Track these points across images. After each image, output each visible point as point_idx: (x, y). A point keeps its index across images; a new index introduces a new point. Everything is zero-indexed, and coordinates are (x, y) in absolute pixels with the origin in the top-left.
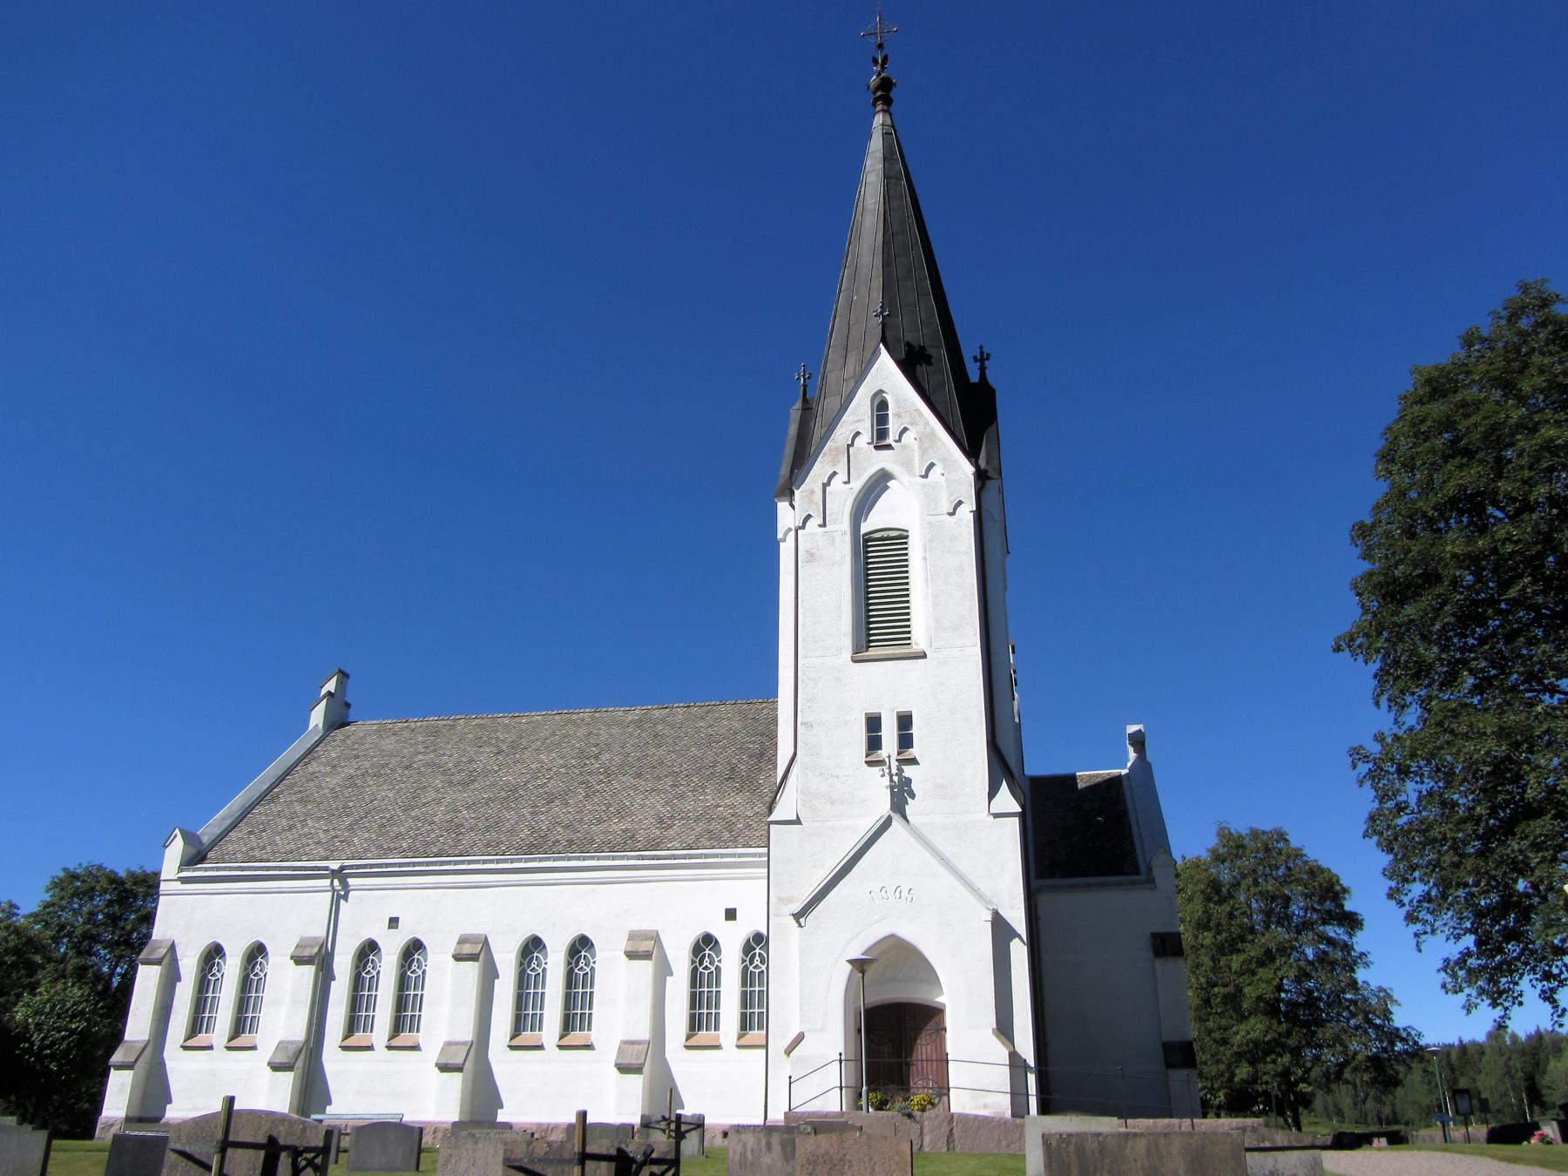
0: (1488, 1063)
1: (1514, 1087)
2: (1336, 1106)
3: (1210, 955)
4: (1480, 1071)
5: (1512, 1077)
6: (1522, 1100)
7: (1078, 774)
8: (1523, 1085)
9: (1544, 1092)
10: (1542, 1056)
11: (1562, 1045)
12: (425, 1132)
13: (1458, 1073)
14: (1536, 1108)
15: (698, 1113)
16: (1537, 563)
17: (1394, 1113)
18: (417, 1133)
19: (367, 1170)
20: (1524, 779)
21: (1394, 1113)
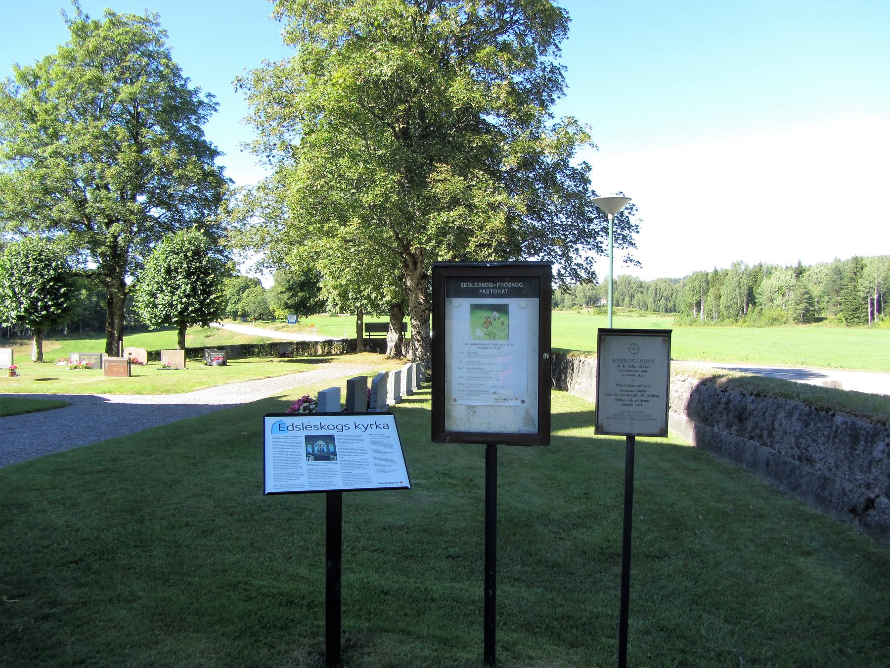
1: (740, 294)
2: (644, 302)
3: (294, 259)
5: (740, 288)
7: (637, 438)
8: (745, 292)
9: (757, 296)
10: (759, 277)
11: (772, 271)
14: (750, 305)
17: (675, 306)
18: (321, 506)
19: (340, 341)
20: (135, 151)
21: (675, 306)
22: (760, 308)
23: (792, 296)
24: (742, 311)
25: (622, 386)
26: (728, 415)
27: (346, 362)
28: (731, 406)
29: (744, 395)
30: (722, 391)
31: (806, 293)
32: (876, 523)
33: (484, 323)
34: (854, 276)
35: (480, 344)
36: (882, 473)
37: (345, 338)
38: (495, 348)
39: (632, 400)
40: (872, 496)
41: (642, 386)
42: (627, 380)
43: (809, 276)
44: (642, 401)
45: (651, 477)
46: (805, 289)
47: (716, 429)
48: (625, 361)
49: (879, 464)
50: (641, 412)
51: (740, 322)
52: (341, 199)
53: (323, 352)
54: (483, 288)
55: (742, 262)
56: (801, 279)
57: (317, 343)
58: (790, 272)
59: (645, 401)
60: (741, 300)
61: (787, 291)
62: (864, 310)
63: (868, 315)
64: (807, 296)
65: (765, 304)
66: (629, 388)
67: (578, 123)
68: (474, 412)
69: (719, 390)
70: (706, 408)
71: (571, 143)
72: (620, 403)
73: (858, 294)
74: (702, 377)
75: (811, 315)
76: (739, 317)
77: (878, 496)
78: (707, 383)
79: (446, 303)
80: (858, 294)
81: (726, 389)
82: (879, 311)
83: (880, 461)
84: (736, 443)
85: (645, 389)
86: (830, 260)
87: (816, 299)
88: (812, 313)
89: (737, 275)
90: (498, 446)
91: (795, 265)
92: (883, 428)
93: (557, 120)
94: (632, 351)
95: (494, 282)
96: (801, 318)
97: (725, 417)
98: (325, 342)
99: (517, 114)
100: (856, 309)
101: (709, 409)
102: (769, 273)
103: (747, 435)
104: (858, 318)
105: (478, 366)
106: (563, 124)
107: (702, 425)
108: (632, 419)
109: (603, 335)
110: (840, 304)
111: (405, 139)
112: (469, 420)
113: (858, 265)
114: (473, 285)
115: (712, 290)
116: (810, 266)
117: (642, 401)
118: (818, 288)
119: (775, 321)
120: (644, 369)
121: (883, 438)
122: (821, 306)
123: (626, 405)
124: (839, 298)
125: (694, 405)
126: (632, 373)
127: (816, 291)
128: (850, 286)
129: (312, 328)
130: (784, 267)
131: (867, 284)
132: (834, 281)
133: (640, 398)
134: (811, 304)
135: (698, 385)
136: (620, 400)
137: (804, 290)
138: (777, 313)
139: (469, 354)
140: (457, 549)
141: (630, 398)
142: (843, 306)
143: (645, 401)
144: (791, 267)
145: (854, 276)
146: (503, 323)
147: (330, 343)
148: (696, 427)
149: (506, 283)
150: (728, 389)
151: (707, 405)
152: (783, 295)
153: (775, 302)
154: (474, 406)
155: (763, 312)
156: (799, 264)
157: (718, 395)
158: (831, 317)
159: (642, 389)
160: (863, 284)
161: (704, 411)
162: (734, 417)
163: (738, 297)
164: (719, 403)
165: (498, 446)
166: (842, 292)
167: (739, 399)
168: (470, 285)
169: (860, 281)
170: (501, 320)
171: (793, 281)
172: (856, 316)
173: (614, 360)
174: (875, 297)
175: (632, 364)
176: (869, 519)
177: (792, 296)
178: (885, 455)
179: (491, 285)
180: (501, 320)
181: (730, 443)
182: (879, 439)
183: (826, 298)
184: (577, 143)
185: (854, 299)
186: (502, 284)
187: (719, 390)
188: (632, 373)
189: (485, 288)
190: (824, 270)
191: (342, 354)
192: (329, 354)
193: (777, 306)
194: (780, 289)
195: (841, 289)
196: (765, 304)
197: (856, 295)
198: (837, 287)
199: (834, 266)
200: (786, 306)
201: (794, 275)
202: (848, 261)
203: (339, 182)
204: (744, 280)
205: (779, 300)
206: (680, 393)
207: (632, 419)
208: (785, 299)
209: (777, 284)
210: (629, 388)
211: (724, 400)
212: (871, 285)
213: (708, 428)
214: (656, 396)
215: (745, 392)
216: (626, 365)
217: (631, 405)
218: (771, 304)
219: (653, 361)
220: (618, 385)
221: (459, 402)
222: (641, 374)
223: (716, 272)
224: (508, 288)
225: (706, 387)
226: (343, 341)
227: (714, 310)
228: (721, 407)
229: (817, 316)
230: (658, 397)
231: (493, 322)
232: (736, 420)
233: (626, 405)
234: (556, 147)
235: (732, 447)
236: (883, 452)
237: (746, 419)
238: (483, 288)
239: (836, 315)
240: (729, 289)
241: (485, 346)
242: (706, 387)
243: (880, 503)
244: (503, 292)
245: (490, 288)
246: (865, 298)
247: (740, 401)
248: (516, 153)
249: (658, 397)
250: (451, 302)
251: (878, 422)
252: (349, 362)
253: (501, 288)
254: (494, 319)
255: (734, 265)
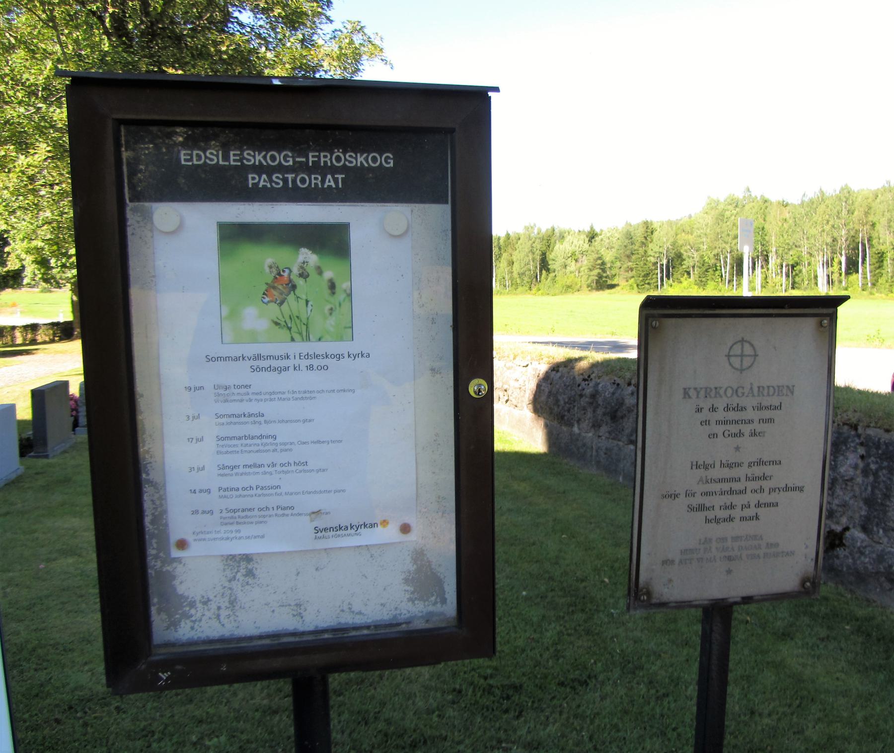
0: (521, 244)
4: (516, 250)
5: (533, 253)
6: (537, 267)
8: (538, 258)
9: (550, 262)
10: (552, 241)
11: (565, 235)
12: (222, 435)
13: (502, 251)
14: (544, 272)
15: (832, 188)
16: (171, 71)
19: (50, 324)
22: (554, 274)
23: (585, 262)
24: (536, 279)
25: (706, 467)
26: (594, 411)
27: (57, 352)
28: (600, 400)
29: (618, 385)
30: (584, 380)
31: (600, 258)
32: (849, 567)
33: (271, 287)
34: (644, 241)
35: (258, 357)
36: (855, 496)
37: (55, 320)
38: (310, 368)
39: (732, 507)
40: (838, 529)
41: (761, 463)
42: (722, 449)
43: (602, 240)
44: (759, 505)
45: (510, 510)
46: (597, 253)
47: (576, 429)
48: (717, 394)
49: (849, 483)
50: (755, 537)
51: (534, 290)
52: (19, 116)
53: (25, 340)
54: (259, 169)
55: (535, 225)
56: (593, 243)
57: (14, 328)
58: (583, 237)
59: (769, 505)
60: (534, 266)
61: (580, 256)
62: (654, 276)
63: (657, 281)
64: (599, 262)
65: (559, 271)
66: (726, 473)
67: (366, 31)
68: (250, 573)
69: (579, 379)
70: (562, 402)
71: (357, 57)
72: (701, 516)
73: (648, 259)
74: (552, 361)
75: (604, 281)
76: (533, 285)
77: (847, 529)
78: (560, 369)
79: (132, 218)
80: (648, 259)
81: (589, 376)
82: (668, 277)
83: (851, 479)
84: (606, 449)
85: (768, 470)
86: (621, 225)
87: (609, 265)
88: (604, 279)
89: (530, 239)
90: (335, 680)
91: (587, 229)
92: (853, 433)
93: (337, 25)
94: (736, 362)
95: (300, 148)
96: (594, 285)
97: (589, 414)
98: (26, 327)
99: (283, 9)
100: (647, 275)
101: (565, 403)
102: (562, 237)
103: (625, 438)
104: (649, 284)
105: (255, 430)
106: (345, 31)
107: (555, 423)
108: (729, 558)
109: (653, 316)
110: (632, 270)
111: (120, 37)
112: (232, 602)
113: (649, 230)
114: (226, 157)
115: (505, 255)
116: (602, 231)
117: (759, 505)
118: (611, 253)
119: (568, 288)
120: (767, 414)
121: (855, 447)
122: (613, 272)
123: (717, 521)
124: (630, 264)
125: (543, 398)
126: (734, 429)
127: (608, 257)
128: (641, 251)
129: (14, 308)
130: (577, 231)
131: (657, 249)
132: (626, 246)
133: (753, 498)
134: (604, 270)
135: (547, 372)
136: (701, 508)
137: (597, 256)
138: (570, 280)
139: (223, 392)
140: (223, 739)
141: (727, 499)
142: (634, 272)
143: (769, 505)
144: (584, 231)
145: (644, 241)
146: (332, 286)
147: (34, 327)
148: (546, 426)
149: (338, 153)
150: (592, 376)
151: (562, 398)
152: (576, 261)
153: (568, 268)
154: (248, 558)
155: (557, 279)
156: (592, 228)
157: (579, 385)
158: (623, 283)
159: (758, 471)
160: (653, 248)
161: (559, 406)
162: (604, 414)
163: (531, 263)
164: (581, 396)
165: (335, 680)
166: (634, 257)
167: (612, 390)
168: (213, 156)
169: (650, 245)
170: (328, 274)
171: (586, 246)
172: (647, 282)
173: (686, 393)
174: (665, 262)
175: (735, 401)
176: (837, 562)
177: (585, 262)
178: (859, 472)
179: (284, 157)
180: (328, 274)
181: (599, 448)
182: (847, 449)
183: (618, 264)
184: (365, 57)
185: (645, 264)
186: (325, 158)
187: (579, 379)
188: (734, 429)
189: (269, 171)
190: (616, 235)
191: (52, 341)
192: (34, 342)
193: (571, 272)
194: (573, 254)
195: (633, 254)
196: (559, 271)
197: (647, 261)
198: (628, 252)
199: (625, 231)
200: (579, 272)
201: (587, 240)
202: (638, 225)
203: (13, 88)
204: (538, 245)
205: (572, 266)
206: (521, 382)
207: (729, 558)
208: (579, 265)
209: (570, 248)
210: (726, 473)
211: (588, 391)
212: (661, 250)
213: (564, 428)
214: (794, 489)
215: (618, 381)
216: (721, 403)
217: (731, 519)
218: (564, 270)
219: (791, 390)
220: (698, 467)
221: (195, 550)
222: (759, 427)
223: (508, 236)
224: (344, 169)
225: (559, 374)
226: (54, 325)
227: (507, 277)
228: (584, 401)
229: (609, 282)
230: (801, 489)
231: (300, 282)
232: (608, 418)
233: (717, 521)
234: (339, 58)
235: (602, 453)
236: (856, 467)
237: (622, 418)
238: (259, 169)
239: (627, 281)
240: (522, 255)
241: (275, 363)
242: (559, 374)
243: (853, 539)
244: (330, 182)
245: (288, 170)
246: (655, 264)
247: (613, 394)
248: (284, 64)
249: (801, 489)
250: (147, 217)
251: (844, 424)
252: (61, 352)
253: (324, 170)
254: (304, 275)
255: (527, 228)
